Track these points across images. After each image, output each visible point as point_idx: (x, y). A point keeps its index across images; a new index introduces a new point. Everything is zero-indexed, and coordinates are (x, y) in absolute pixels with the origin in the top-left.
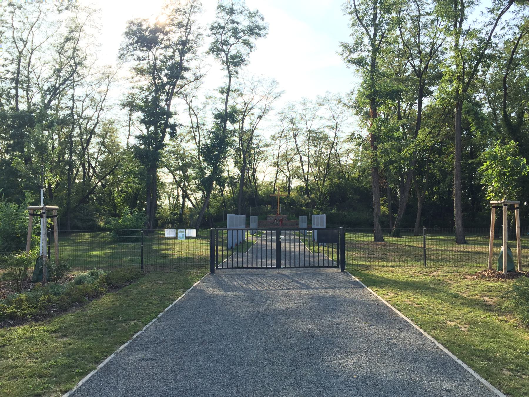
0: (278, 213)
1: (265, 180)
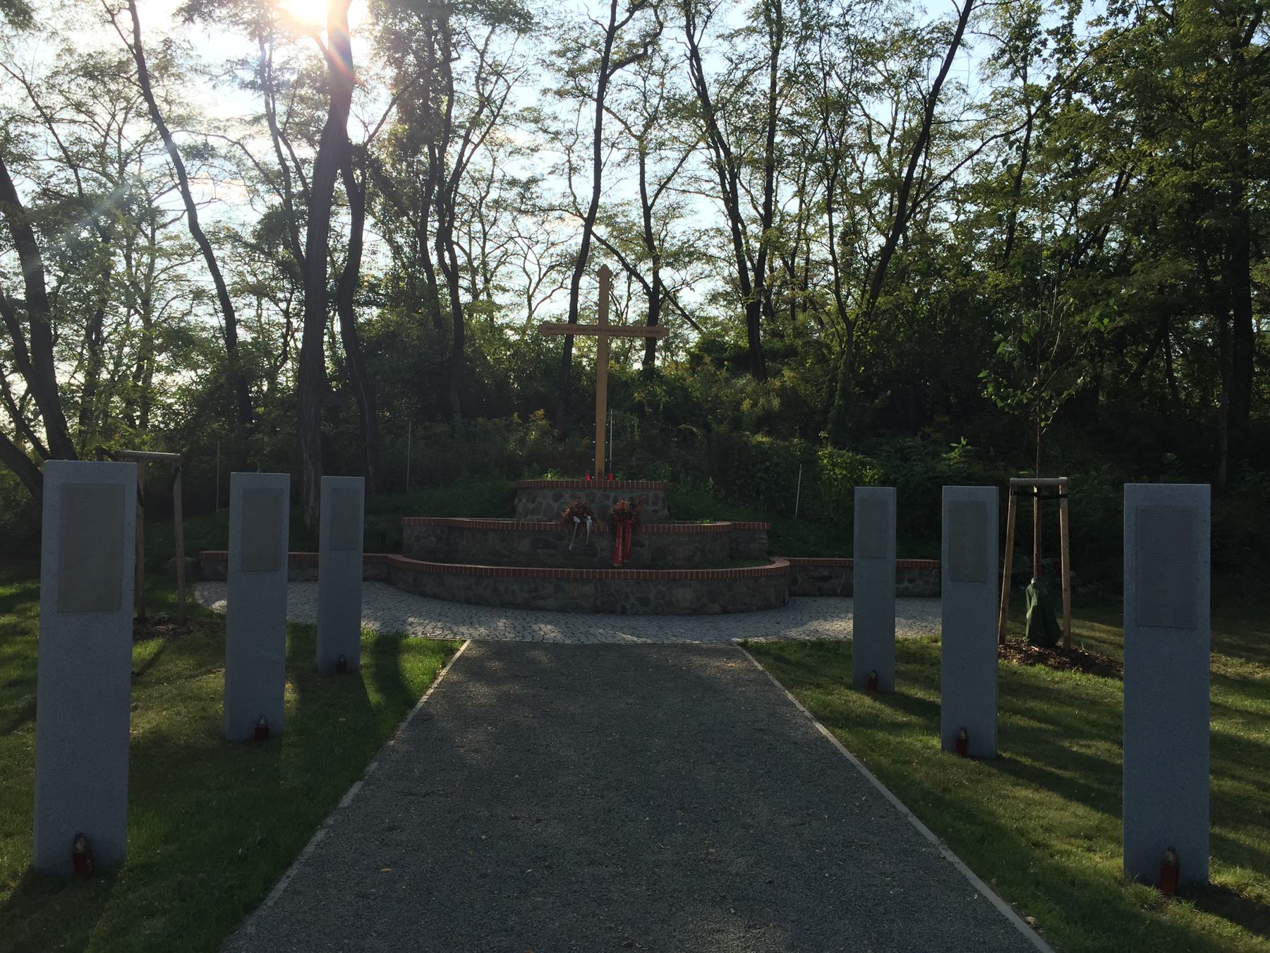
0: (600, 462)
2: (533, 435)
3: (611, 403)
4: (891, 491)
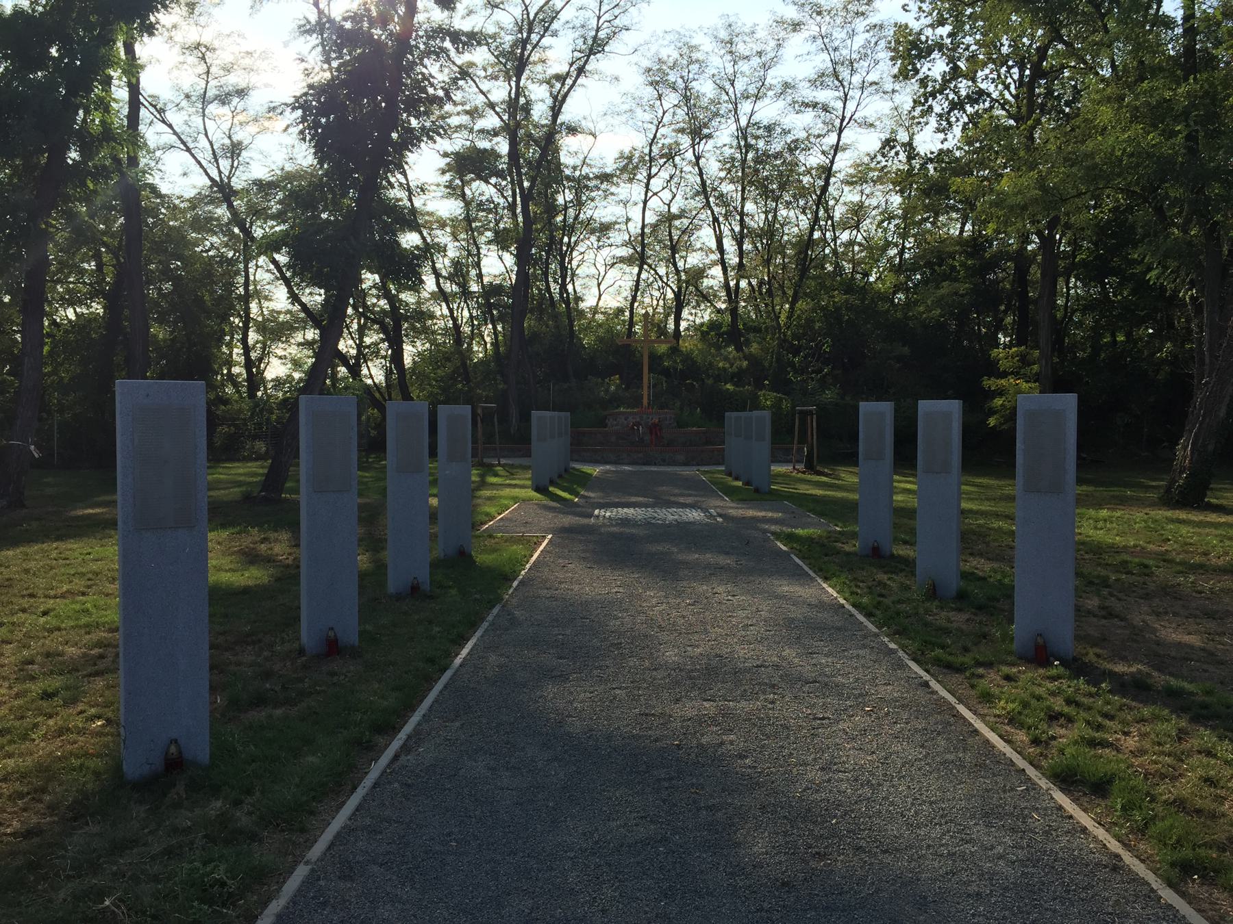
0: (645, 401)
1: (601, 304)
2: (613, 388)
3: (651, 370)
4: (1068, 402)
